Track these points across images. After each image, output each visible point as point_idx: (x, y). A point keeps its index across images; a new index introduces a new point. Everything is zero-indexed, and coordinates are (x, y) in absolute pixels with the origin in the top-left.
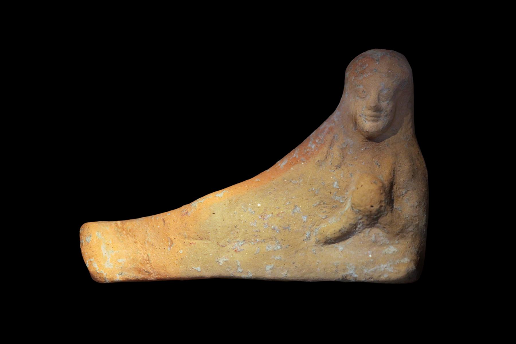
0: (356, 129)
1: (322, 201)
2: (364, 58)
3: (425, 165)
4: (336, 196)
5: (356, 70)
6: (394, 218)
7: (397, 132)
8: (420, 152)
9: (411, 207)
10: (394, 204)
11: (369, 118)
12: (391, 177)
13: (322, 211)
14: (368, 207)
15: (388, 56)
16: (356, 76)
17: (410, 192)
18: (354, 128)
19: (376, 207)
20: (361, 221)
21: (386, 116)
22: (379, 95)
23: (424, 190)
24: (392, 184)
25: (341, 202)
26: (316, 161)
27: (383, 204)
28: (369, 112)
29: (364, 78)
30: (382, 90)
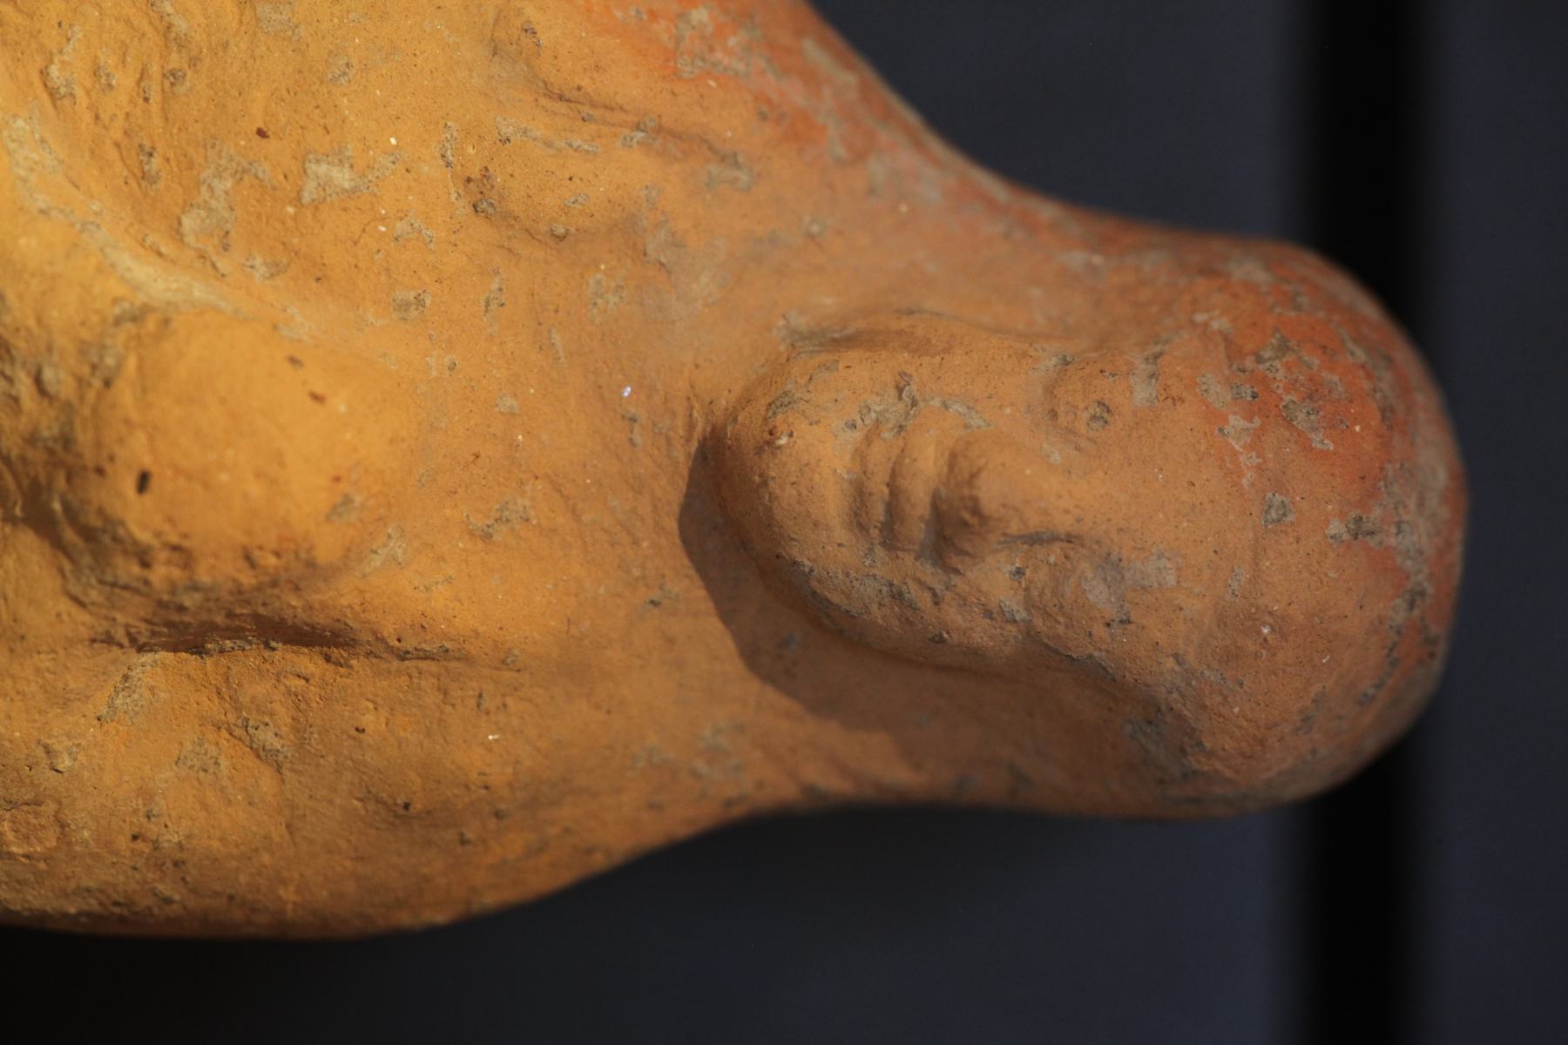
0: (798, 339)
1: (194, 62)
2: (1386, 411)
3: (490, 900)
4: (240, 175)
5: (1283, 348)
6: (45, 661)
7: (767, 678)
8: (599, 862)
9: (145, 793)
10: (163, 655)
11: (879, 456)
12: (388, 631)
13: (109, 60)
14: (138, 451)
15: (1398, 613)
16: (1233, 351)
17: (267, 783)
18: (801, 322)
19: (139, 517)
20: (24, 387)
21: (898, 596)
22: (1069, 539)
23: (288, 894)
24: (328, 639)
25: (188, 222)
26: (531, 12)
27: (162, 573)
28: (927, 467)
29: (1215, 418)
30: (1111, 565)
